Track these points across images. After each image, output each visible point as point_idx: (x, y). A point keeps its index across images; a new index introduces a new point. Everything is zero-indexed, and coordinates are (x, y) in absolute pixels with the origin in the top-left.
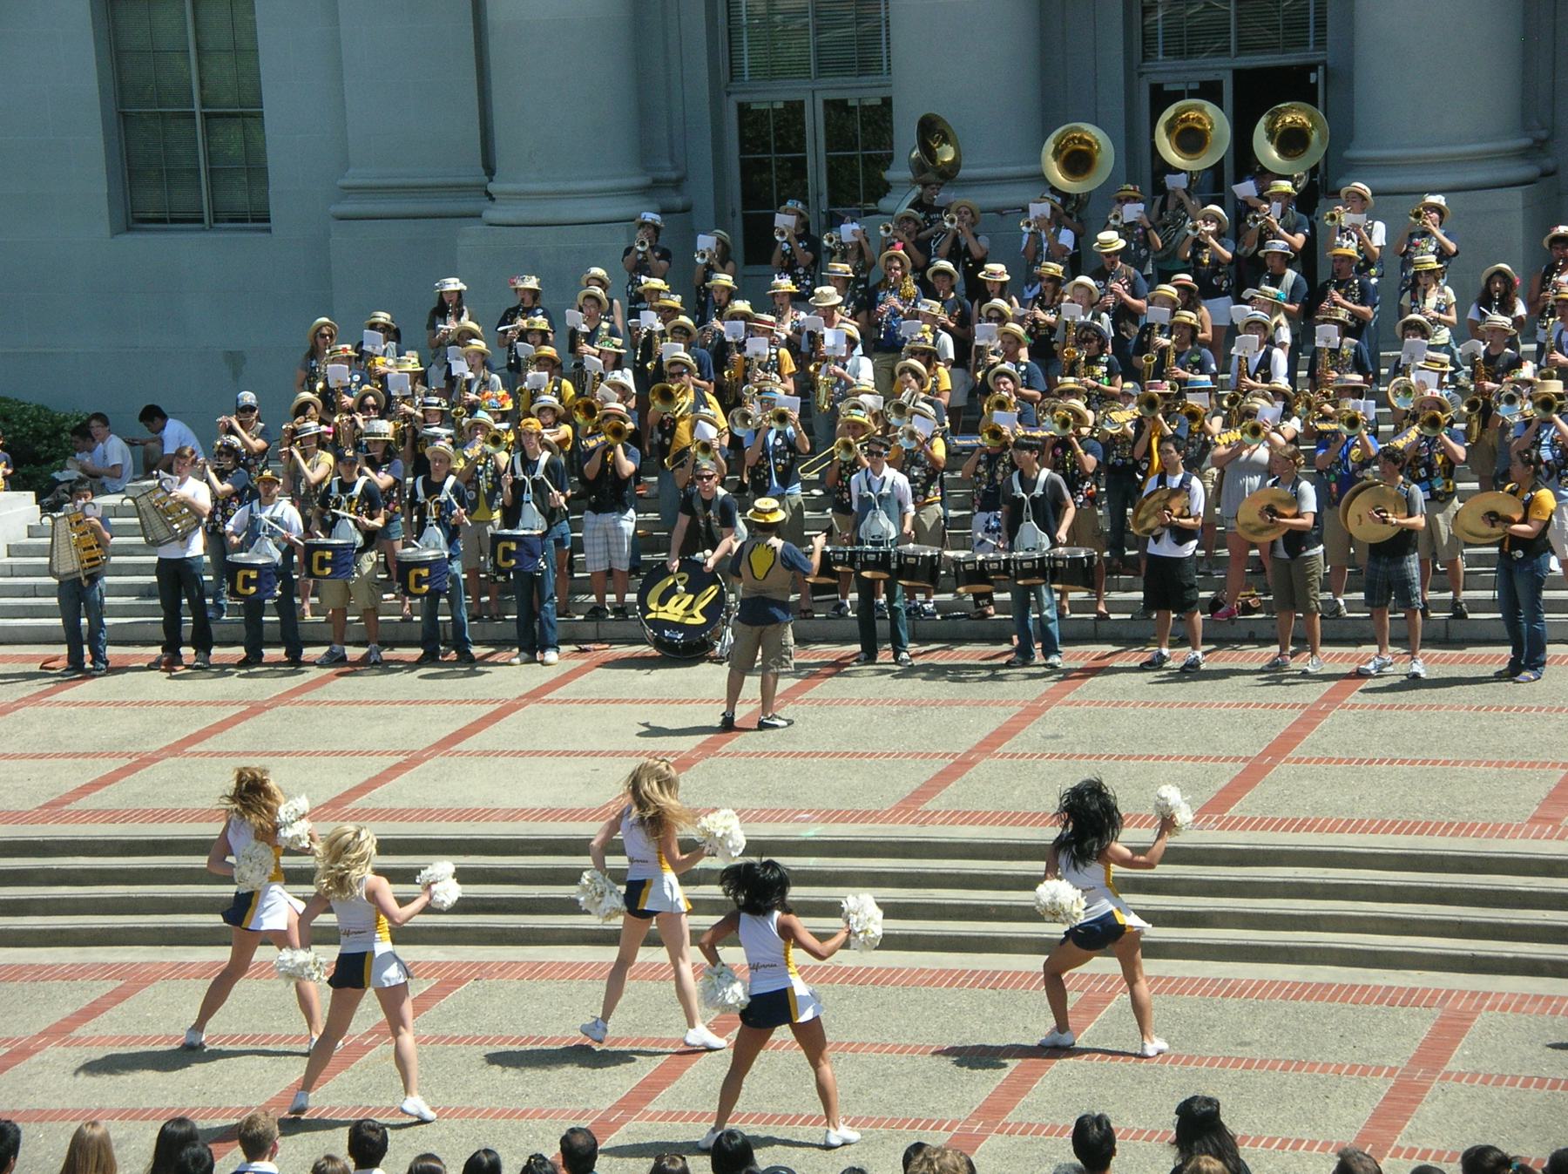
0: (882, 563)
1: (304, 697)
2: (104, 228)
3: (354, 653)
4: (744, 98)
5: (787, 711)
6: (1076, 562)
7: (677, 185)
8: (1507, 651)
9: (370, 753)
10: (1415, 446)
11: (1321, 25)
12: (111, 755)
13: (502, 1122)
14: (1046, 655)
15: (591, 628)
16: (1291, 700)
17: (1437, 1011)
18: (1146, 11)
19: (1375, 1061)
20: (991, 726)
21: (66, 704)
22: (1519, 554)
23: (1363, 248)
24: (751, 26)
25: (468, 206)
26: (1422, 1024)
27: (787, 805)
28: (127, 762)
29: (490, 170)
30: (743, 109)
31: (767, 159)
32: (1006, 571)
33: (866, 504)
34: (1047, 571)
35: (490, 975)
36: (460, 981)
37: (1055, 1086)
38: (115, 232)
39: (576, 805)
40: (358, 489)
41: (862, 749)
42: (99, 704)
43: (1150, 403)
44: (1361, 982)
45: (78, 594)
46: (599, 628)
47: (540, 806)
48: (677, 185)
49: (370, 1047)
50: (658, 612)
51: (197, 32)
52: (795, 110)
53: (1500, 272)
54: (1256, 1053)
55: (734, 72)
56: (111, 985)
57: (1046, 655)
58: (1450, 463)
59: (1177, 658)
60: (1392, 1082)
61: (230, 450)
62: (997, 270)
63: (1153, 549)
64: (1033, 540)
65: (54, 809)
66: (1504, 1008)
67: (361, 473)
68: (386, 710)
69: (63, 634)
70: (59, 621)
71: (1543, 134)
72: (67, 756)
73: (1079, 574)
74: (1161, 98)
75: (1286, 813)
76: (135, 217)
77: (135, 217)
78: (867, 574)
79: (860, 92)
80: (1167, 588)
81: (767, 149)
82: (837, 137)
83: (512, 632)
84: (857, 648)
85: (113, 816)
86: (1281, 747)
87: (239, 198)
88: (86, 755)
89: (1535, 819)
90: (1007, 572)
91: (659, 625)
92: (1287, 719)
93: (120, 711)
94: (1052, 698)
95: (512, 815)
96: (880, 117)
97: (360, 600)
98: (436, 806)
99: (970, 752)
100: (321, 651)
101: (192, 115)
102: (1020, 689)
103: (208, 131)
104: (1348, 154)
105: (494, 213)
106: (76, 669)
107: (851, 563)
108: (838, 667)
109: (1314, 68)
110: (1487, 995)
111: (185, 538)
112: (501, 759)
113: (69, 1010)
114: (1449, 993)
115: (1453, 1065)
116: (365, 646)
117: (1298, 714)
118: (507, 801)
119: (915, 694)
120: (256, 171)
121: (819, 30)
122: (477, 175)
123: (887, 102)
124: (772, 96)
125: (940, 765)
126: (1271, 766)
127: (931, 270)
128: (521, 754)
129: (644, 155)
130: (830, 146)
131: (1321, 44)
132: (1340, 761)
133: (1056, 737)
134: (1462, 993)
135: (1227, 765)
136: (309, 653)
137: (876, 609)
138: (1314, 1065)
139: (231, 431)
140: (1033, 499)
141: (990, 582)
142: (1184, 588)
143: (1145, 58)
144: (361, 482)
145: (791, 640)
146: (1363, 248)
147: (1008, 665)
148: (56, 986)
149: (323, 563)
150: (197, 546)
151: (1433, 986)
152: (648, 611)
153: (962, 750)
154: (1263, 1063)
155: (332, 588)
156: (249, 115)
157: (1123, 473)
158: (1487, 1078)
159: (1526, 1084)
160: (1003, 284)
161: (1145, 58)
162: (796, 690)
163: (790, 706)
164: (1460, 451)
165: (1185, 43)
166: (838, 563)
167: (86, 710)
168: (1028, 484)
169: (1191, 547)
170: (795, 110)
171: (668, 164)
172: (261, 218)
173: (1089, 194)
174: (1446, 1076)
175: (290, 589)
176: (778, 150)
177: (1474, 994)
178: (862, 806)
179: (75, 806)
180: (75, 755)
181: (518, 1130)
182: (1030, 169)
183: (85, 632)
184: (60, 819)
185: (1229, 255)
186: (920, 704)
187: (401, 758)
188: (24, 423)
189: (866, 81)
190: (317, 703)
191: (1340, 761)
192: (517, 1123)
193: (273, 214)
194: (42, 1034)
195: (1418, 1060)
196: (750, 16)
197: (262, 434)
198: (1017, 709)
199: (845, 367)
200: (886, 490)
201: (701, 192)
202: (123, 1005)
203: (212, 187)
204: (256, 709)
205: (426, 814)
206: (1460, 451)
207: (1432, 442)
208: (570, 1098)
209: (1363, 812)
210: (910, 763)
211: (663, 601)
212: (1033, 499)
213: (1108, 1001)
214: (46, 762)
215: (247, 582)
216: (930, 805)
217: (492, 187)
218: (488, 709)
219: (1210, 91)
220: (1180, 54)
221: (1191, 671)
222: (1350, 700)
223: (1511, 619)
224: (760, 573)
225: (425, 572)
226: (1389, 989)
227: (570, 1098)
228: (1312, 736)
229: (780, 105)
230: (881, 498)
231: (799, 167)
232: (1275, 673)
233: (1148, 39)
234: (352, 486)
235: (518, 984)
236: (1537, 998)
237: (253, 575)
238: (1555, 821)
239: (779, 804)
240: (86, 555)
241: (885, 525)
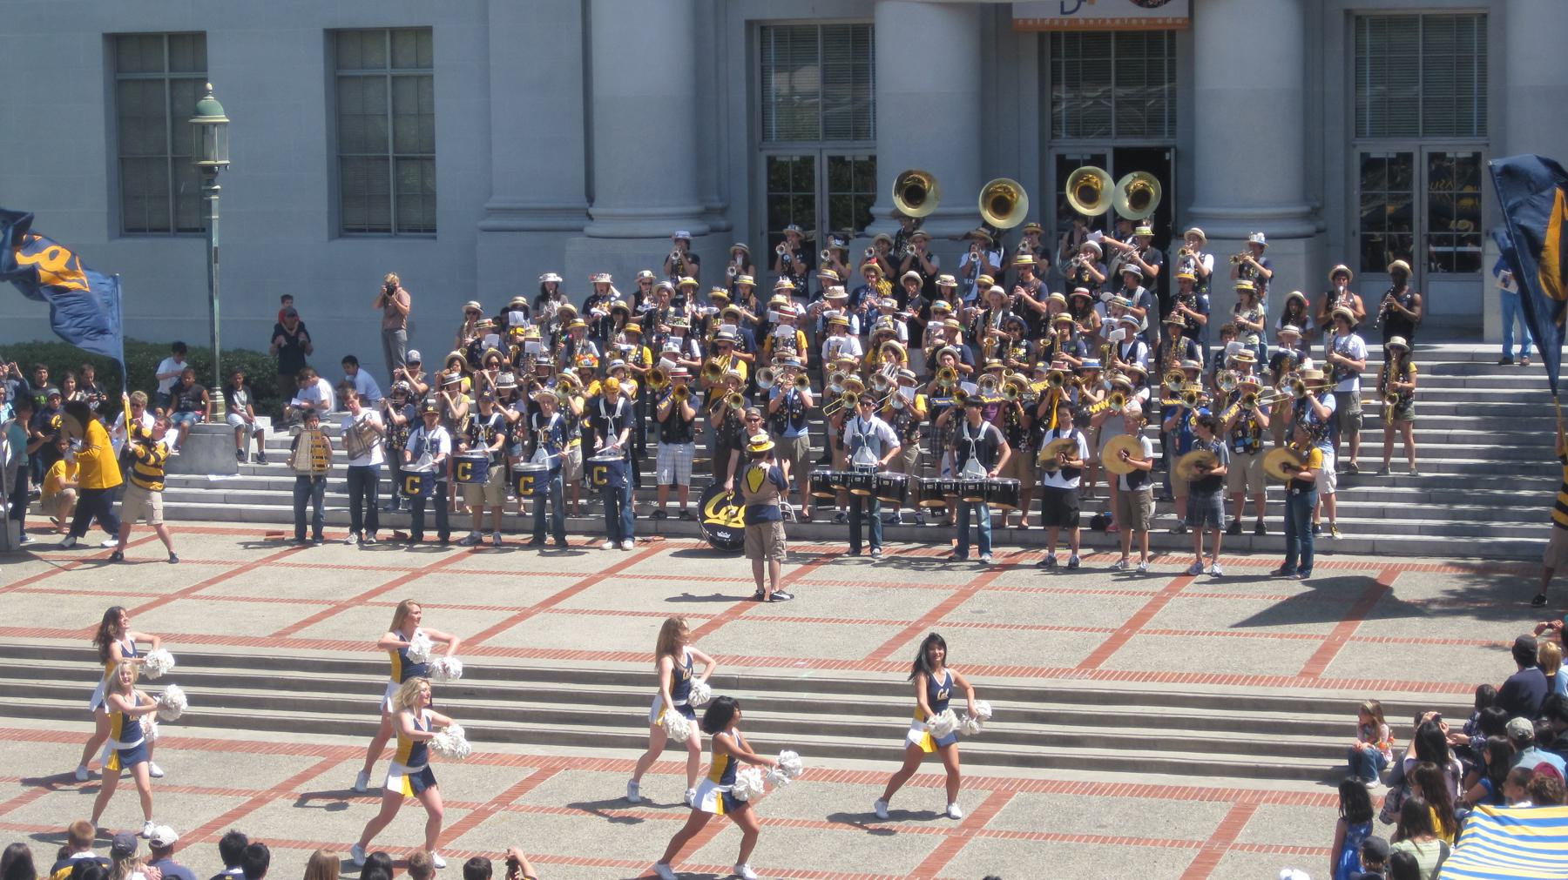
0: (866, 483)
1: (450, 567)
2: (325, 235)
3: (487, 538)
4: (771, 153)
5: (790, 589)
6: (1005, 487)
7: (723, 212)
8: (1283, 557)
9: (494, 608)
10: (1239, 415)
11: (1173, 121)
12: (317, 602)
13: (583, 868)
14: (981, 553)
15: (652, 525)
16: (1144, 589)
17: (1231, 804)
18: (1054, 104)
19: (1189, 838)
20: (935, 603)
21: (288, 565)
22: (1297, 491)
23: (1199, 273)
24: (778, 104)
25: (574, 223)
26: (1219, 813)
27: (789, 655)
28: (326, 607)
29: (590, 198)
30: (771, 161)
31: (787, 194)
32: (956, 491)
33: (857, 442)
34: (985, 492)
35: (576, 767)
36: (555, 770)
37: (971, 855)
38: (331, 238)
39: (639, 650)
40: (492, 422)
41: (843, 612)
42: (310, 566)
43: (1056, 379)
44: (1183, 784)
45: (309, 487)
46: (659, 526)
47: (612, 650)
48: (723, 212)
49: (492, 812)
50: (712, 517)
51: (394, 98)
52: (807, 162)
53: (1296, 298)
54: (1110, 832)
55: (766, 135)
56: (318, 760)
57: (981, 553)
58: (1258, 430)
59: (1063, 556)
60: (1198, 851)
61: (404, 392)
62: (949, 279)
63: (1049, 482)
64: (976, 472)
65: (280, 637)
66: (1275, 801)
67: (495, 409)
68: (507, 578)
69: (293, 517)
70: (291, 508)
71: (1317, 204)
72: (288, 601)
73: (1005, 496)
74: (1065, 166)
75: (1138, 668)
76: (345, 229)
77: (345, 229)
78: (855, 491)
79: (854, 151)
80: (1058, 511)
81: (786, 188)
82: (837, 182)
83: (603, 525)
84: (848, 545)
85: (319, 644)
86: (1136, 623)
87: (415, 215)
88: (301, 601)
89: (1302, 674)
90: (960, 490)
91: (715, 528)
92: (1141, 603)
93: (323, 571)
94: (979, 584)
95: (593, 656)
96: (867, 169)
97: (492, 500)
98: (540, 647)
99: (920, 621)
100: (465, 534)
101: (387, 159)
102: (962, 576)
103: (397, 168)
104: (1193, 209)
105: (591, 229)
106: (301, 541)
107: (844, 484)
108: (832, 557)
109: (1168, 149)
110: (1264, 793)
111: (368, 450)
112: (586, 616)
113: (291, 775)
114: (1240, 791)
115: (1239, 839)
116: (489, 533)
117: (1149, 599)
118: (590, 646)
119: (882, 579)
120: (429, 197)
121: (826, 107)
122: (579, 200)
123: (873, 159)
124: (791, 153)
125: (899, 629)
126: (1129, 635)
127: (902, 279)
128: (601, 612)
129: (700, 189)
130: (831, 189)
131: (1172, 133)
132: (1176, 633)
133: (980, 612)
134: (1248, 792)
135: (1099, 634)
136: (454, 535)
137: (857, 514)
138: (1148, 840)
139: (403, 377)
140: (977, 443)
141: (943, 499)
142: (1070, 510)
143: (1053, 136)
144: (495, 416)
145: (783, 536)
146: (1199, 273)
147: (950, 560)
148: (282, 757)
149: (465, 471)
150: (377, 457)
151: (1230, 787)
152: (705, 517)
153: (914, 619)
154: (1114, 839)
155: (472, 489)
156: (425, 158)
157: (1025, 425)
158: (1261, 847)
159: (1285, 851)
160: (953, 289)
161: (1053, 136)
162: (799, 573)
163: (793, 585)
164: (1265, 420)
165: (1079, 129)
166: (834, 483)
167: (302, 570)
168: (974, 431)
169: (1075, 483)
170: (807, 162)
171: (716, 197)
172: (430, 229)
173: (1009, 230)
174: (1234, 847)
175: (443, 489)
176: (795, 189)
177: (1256, 792)
178: (842, 658)
179: (294, 636)
180: (294, 601)
181: (595, 874)
182: (972, 209)
183: (309, 517)
184: (283, 645)
185: (1103, 277)
186: (886, 586)
187: (516, 613)
188: (265, 370)
189: (857, 144)
190: (458, 571)
191: (1176, 633)
192: (594, 868)
193: (440, 225)
194: (273, 789)
195: (1217, 836)
196: (777, 96)
197: (425, 380)
198: (953, 591)
199: (853, 339)
200: (872, 432)
201: (739, 216)
202: (325, 774)
203: (398, 205)
204: (416, 574)
205: (533, 653)
206: (1265, 420)
207: (1248, 412)
208: (631, 853)
209: (1191, 668)
210: (877, 628)
211: (716, 511)
212: (977, 443)
213: (1010, 796)
214: (275, 605)
215: (413, 485)
216: (890, 658)
217: (591, 211)
218: (578, 580)
219: (1099, 161)
220: (1077, 135)
221: (1073, 568)
222: (1184, 590)
223: (1290, 538)
224: (754, 489)
225: (531, 480)
226: (1201, 789)
227: (631, 853)
228: (1158, 615)
229: (796, 159)
230: (868, 438)
231: (809, 202)
232: (1120, 572)
233: (1055, 123)
234: (489, 418)
235: (595, 774)
236: (1296, 794)
237: (417, 480)
238: (1315, 675)
239: (782, 654)
240: (319, 461)
241: (870, 458)
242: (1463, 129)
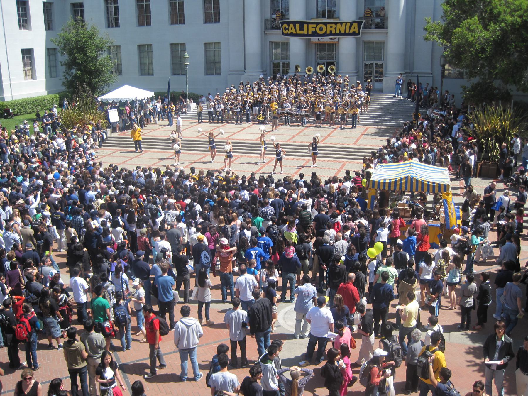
7: (266, 71)
29: (245, 69)
52: (279, 63)
79: (286, 62)
87: (218, 72)
105: (245, 74)
118: (245, 138)
120: (220, 69)
129: (262, 68)
242: (380, 60)
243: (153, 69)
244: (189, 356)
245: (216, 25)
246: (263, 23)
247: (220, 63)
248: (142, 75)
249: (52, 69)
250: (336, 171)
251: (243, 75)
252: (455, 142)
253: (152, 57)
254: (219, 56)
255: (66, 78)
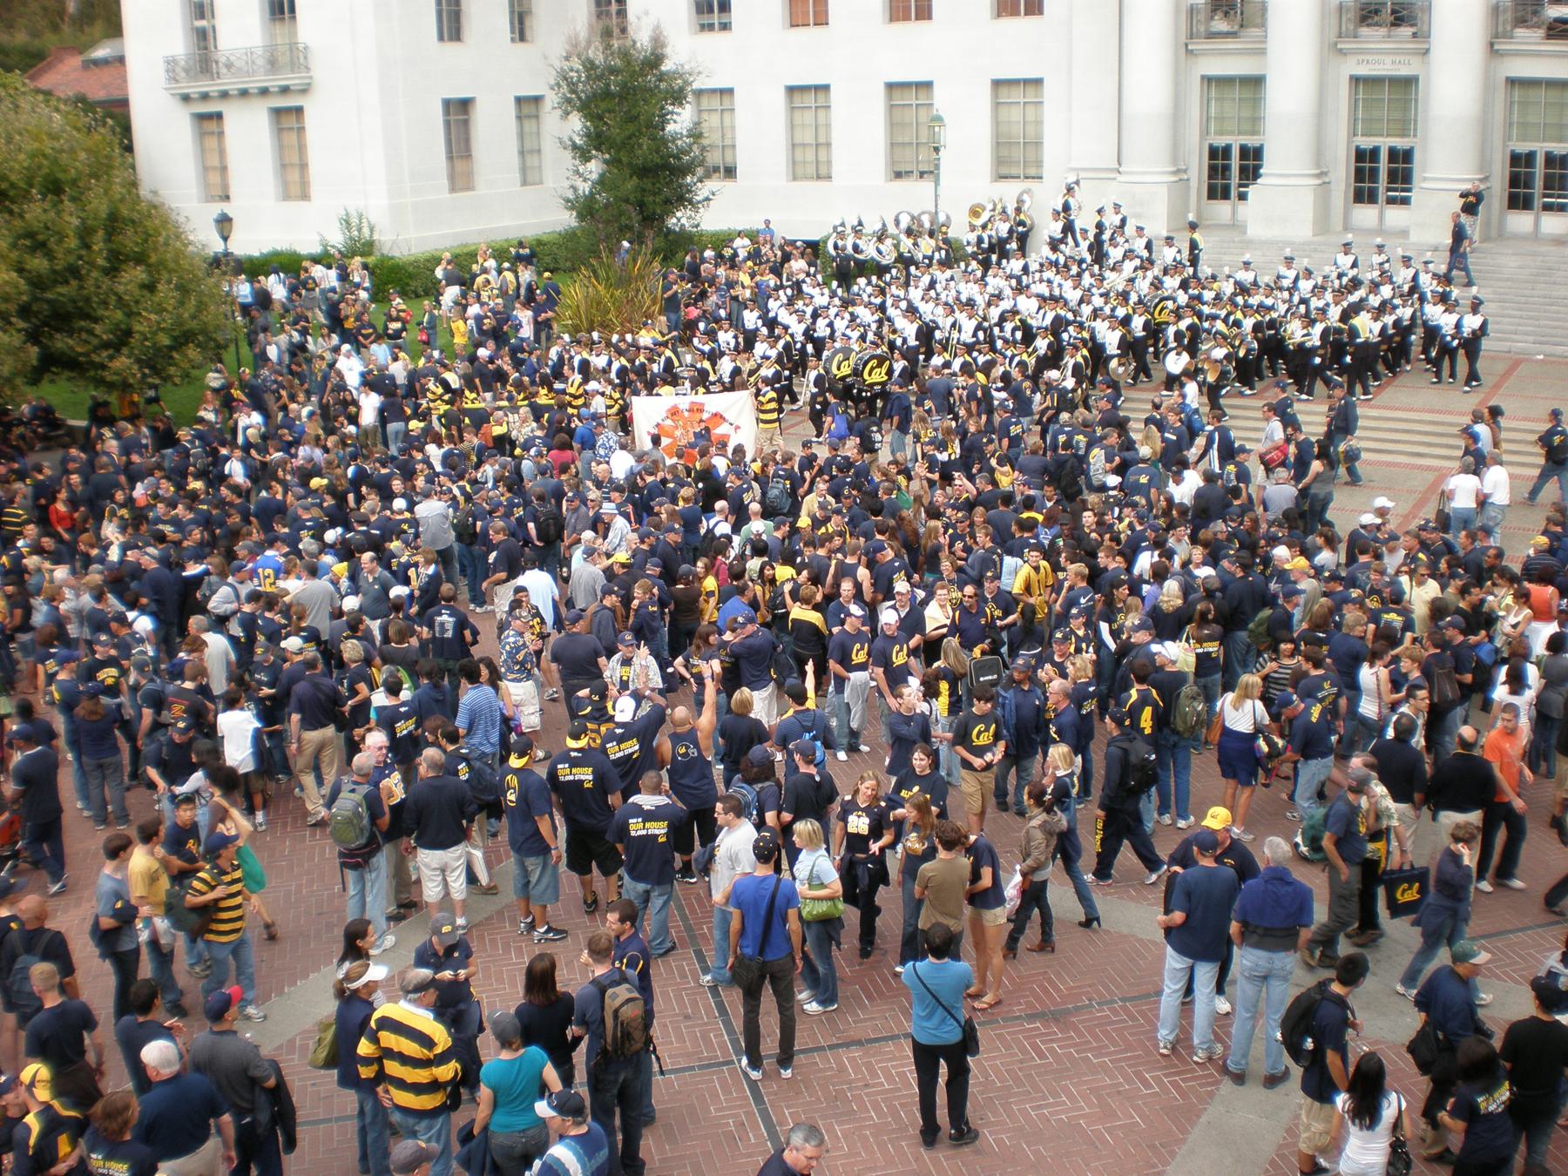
7: (1185, 171)
87: (1032, 172)
105: (1121, 178)
120: (1039, 163)
129: (1175, 159)
242: (1254, 133)
243: (829, 163)
244: (1522, 1147)
245: (1033, 20)
246: (1183, 17)
247: (1038, 144)
248: (795, 179)
249: (296, 160)
250: (1417, 496)
251: (1114, 183)
252: (519, 385)
253: (828, 126)
254: (1039, 123)
255: (575, 189)
